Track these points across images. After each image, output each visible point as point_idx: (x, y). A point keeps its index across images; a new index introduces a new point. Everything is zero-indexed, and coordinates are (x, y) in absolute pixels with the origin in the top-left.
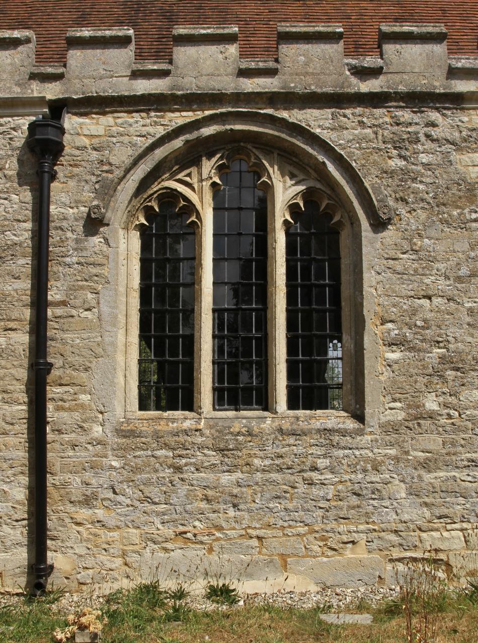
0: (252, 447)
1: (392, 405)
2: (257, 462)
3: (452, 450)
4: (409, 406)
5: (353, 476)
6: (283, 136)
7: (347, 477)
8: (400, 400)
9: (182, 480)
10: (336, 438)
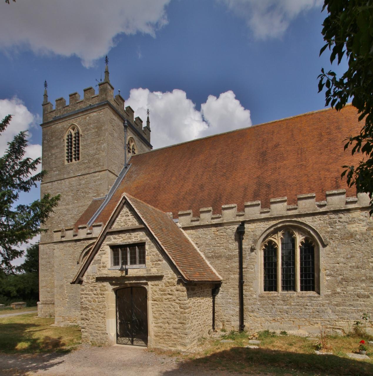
1: (328, 290)
4: (332, 291)
6: (299, 225)
8: (330, 289)
10: (312, 298)
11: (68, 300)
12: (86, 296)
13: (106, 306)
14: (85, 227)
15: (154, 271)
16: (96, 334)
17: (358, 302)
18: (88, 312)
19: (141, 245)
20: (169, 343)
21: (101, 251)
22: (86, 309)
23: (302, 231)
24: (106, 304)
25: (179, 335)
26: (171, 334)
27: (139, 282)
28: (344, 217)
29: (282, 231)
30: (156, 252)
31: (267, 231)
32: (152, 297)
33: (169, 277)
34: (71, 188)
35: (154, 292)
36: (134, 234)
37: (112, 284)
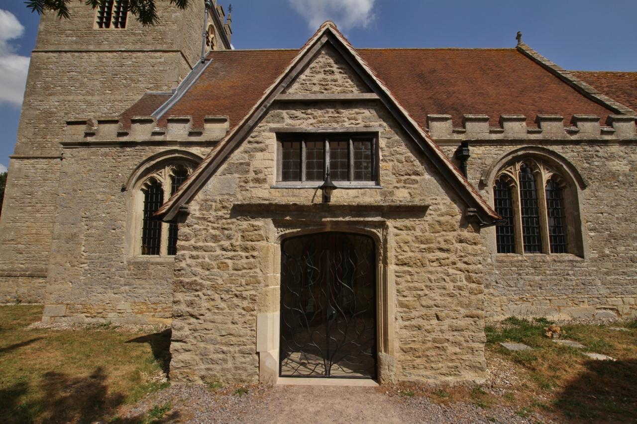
0: (545, 266)
1: (593, 252)
2: (548, 272)
3: (616, 268)
4: (599, 252)
5: (582, 277)
6: (547, 155)
7: (579, 278)
8: (596, 250)
9: (522, 278)
10: (575, 264)
11: (87, 268)
12: (194, 253)
13: (261, 279)
14: (150, 121)
15: (402, 196)
16: (221, 356)
17: (633, 269)
18: (198, 296)
19: (370, 137)
20: (440, 365)
21: (250, 142)
22: (192, 287)
23: (549, 165)
24: (260, 274)
25: (465, 344)
26: (446, 344)
27: (362, 219)
28: (602, 151)
29: (521, 162)
30: (407, 155)
31: (503, 160)
32: (396, 256)
33: (439, 210)
34: (102, 68)
35: (402, 244)
36: (346, 113)
37: (278, 224)
